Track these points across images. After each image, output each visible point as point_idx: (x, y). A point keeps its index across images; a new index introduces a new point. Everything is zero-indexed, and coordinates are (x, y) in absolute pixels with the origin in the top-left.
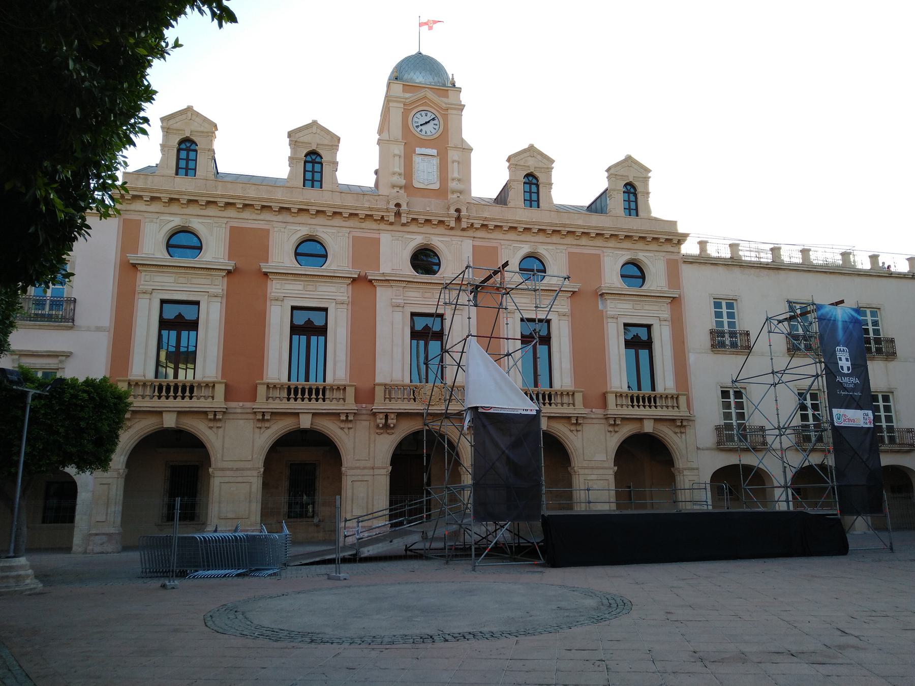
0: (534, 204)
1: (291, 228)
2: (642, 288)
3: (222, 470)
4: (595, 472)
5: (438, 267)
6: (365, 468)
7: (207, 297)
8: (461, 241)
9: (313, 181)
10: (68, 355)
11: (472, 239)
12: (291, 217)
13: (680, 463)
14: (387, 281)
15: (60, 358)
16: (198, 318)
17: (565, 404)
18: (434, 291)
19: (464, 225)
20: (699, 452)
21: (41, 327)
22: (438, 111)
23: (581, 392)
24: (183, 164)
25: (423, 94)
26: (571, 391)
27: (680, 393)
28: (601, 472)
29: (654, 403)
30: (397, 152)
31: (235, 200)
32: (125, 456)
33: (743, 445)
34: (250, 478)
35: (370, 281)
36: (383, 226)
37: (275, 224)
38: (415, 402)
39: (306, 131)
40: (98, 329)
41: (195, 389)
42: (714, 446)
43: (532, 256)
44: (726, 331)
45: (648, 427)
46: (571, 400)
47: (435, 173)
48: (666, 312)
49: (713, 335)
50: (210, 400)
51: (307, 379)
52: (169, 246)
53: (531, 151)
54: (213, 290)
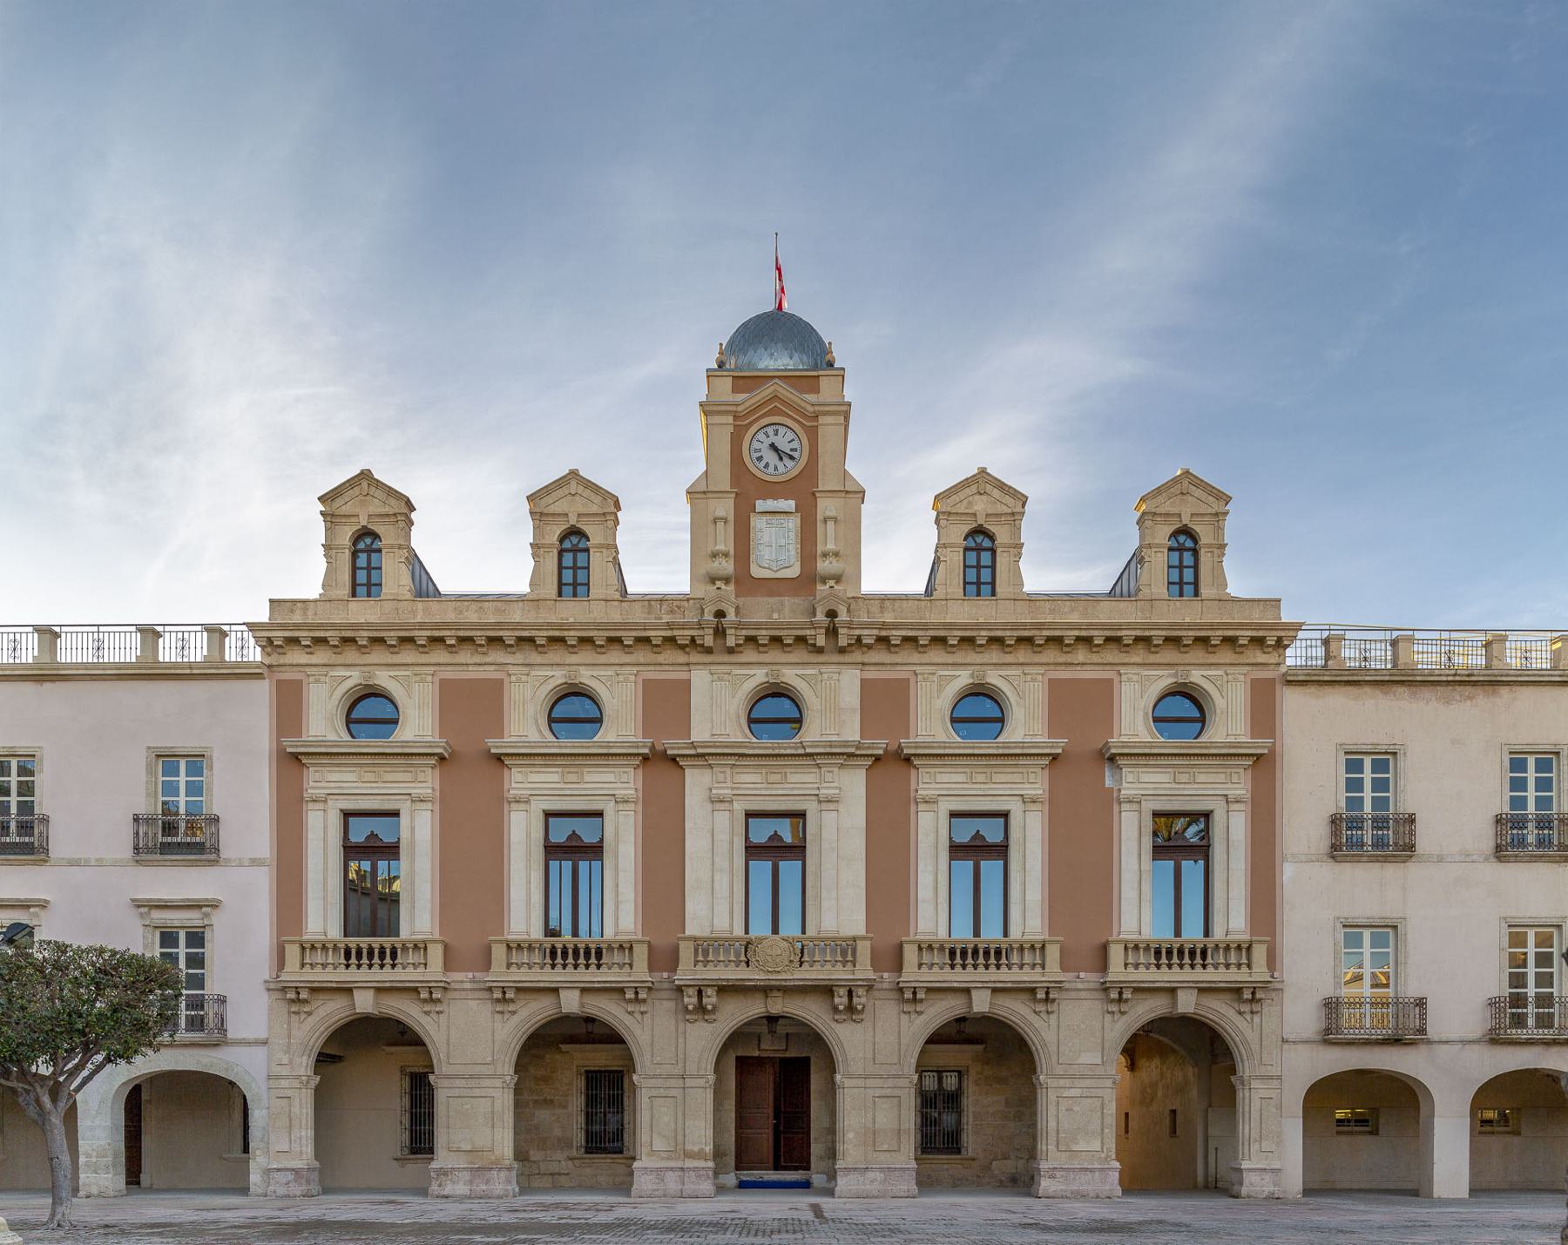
0: (1188, 589)
1: (539, 673)
2: (997, 740)
3: (448, 1077)
4: (1077, 1083)
5: (1200, 724)
6: (670, 1077)
7: (409, 802)
8: (839, 673)
9: (978, 583)
10: (214, 905)
11: (860, 666)
12: (805, 650)
13: (1246, 1069)
14: (704, 757)
15: (204, 909)
16: (602, 840)
17: (700, 963)
18: (788, 770)
19: (843, 641)
20: (1286, 1046)
21: (175, 864)
22: (799, 422)
23: (1058, 942)
24: (568, 576)
25: (769, 391)
26: (1244, 942)
27: (1254, 938)
28: (1088, 1083)
29: (630, 959)
30: (720, 513)
31: (620, 632)
32: (310, 1057)
33: (1547, 1034)
34: (491, 1090)
35: (673, 759)
36: (695, 657)
37: (512, 669)
38: (748, 966)
39: (560, 493)
40: (255, 862)
41: (399, 952)
42: (1318, 1038)
43: (979, 691)
44: (1530, 816)
45: (1187, 1003)
46: (1038, 958)
47: (791, 547)
48: (1242, 786)
49: (1336, 825)
50: (421, 969)
51: (575, 933)
52: (349, 721)
53: (982, 481)
54: (1030, 791)
